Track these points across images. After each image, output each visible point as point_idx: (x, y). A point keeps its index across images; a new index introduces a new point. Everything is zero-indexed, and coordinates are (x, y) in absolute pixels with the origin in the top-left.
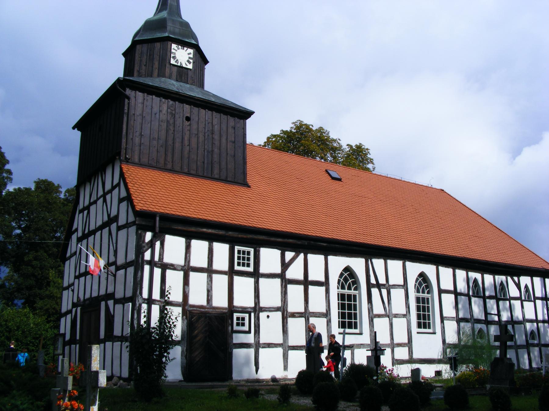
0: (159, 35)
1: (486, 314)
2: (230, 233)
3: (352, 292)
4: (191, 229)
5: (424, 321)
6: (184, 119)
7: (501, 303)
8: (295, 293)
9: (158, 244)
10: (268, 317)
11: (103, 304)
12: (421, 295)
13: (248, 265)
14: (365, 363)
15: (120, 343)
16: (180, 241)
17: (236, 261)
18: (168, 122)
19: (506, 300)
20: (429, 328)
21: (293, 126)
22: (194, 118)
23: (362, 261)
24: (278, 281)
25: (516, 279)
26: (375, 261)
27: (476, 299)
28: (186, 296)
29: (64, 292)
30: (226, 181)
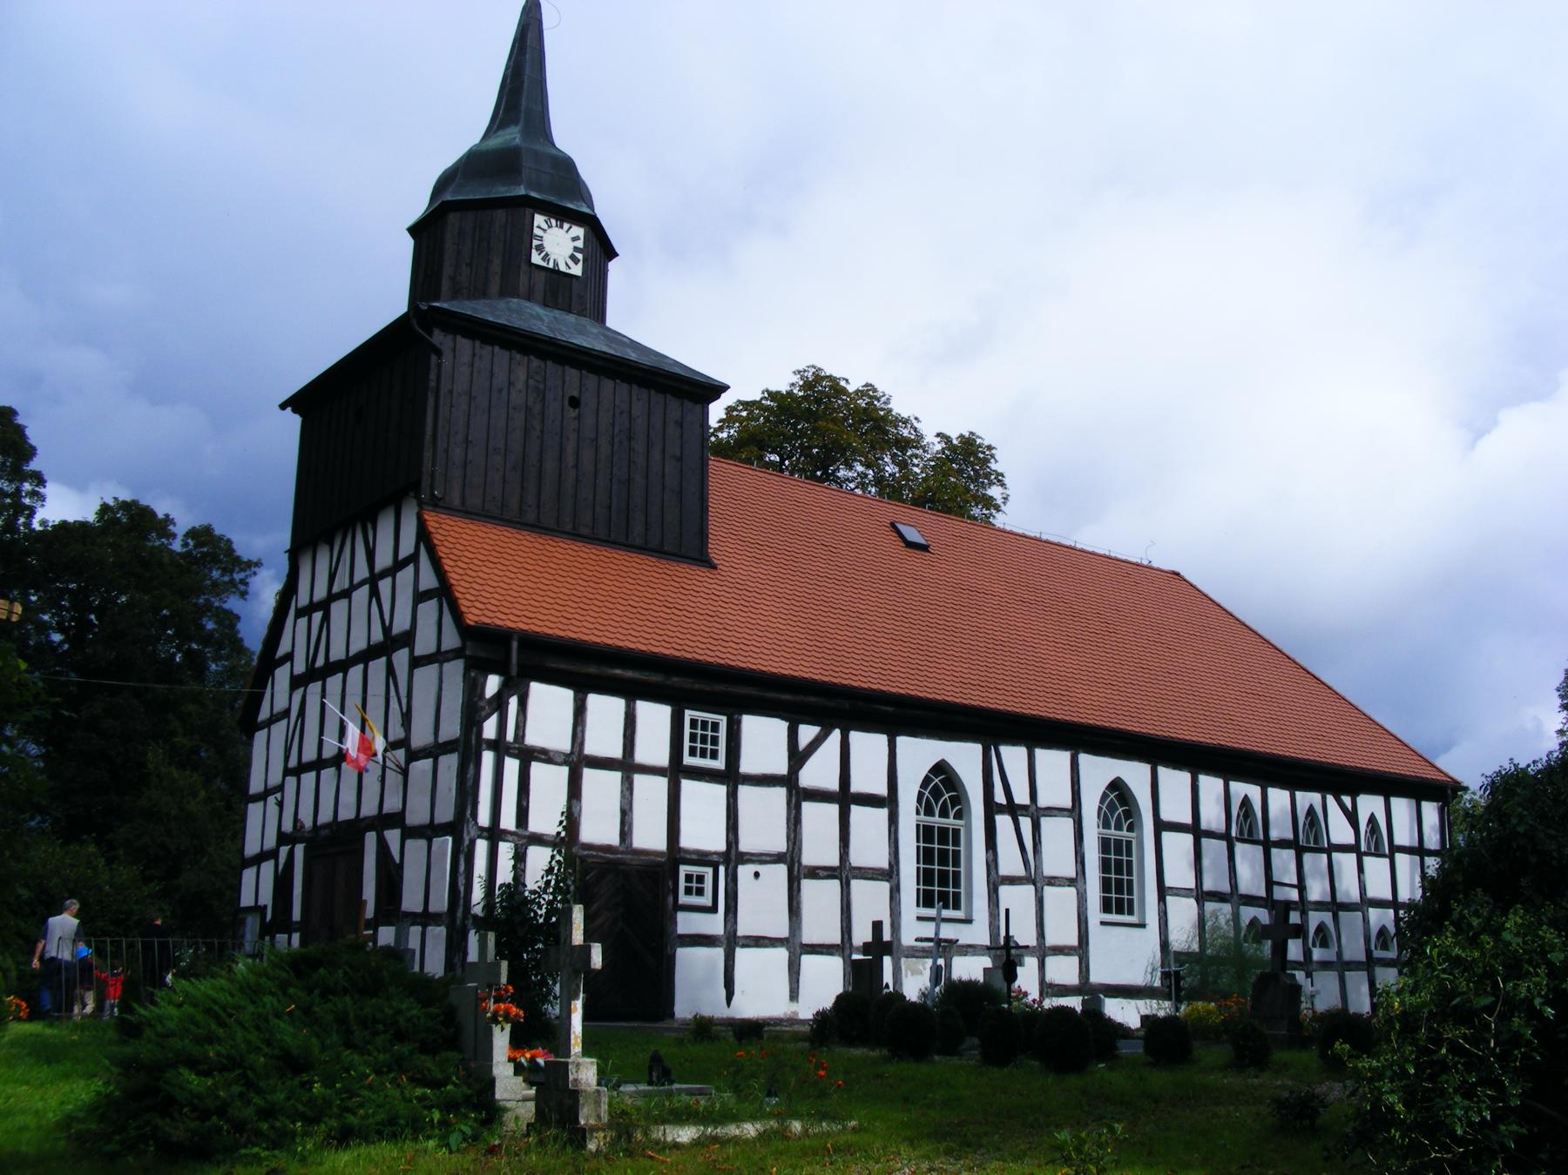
0: (503, 191)
1: (1270, 883)
2: (675, 679)
3: (950, 822)
8: (820, 819)
9: (513, 702)
10: (757, 875)
11: (371, 839)
12: (1112, 833)
13: (714, 755)
16: (563, 697)
17: (687, 744)
18: (528, 409)
19: (1320, 850)
20: (1131, 912)
21: (796, 379)
22: (589, 400)
23: (975, 749)
24: (780, 793)
25: (1347, 800)
27: (1247, 846)
28: (572, 820)
29: (251, 806)
30: (660, 552)
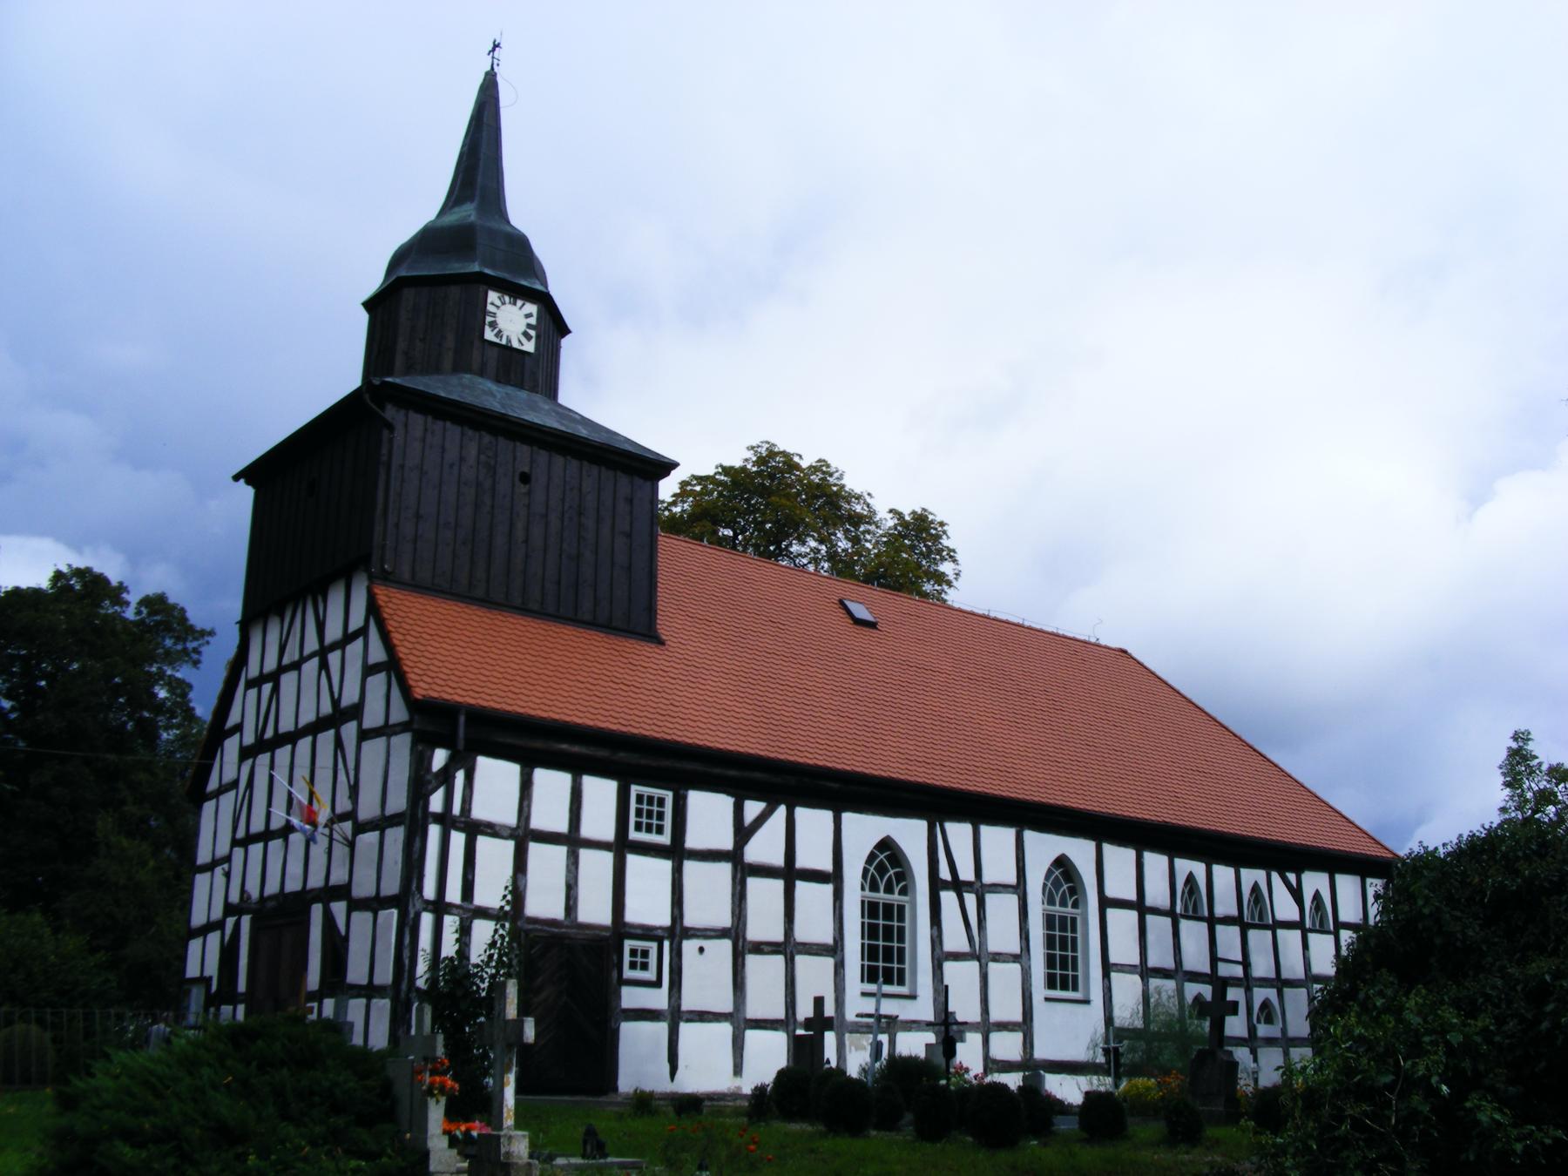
1: (1214, 959)
3: (895, 898)
4: (536, 744)
5: (1063, 974)
6: (517, 479)
7: (1253, 935)
8: (765, 895)
9: (460, 776)
10: (701, 950)
11: (317, 911)
13: (660, 830)
14: (922, 1054)
15: (364, 1001)
17: (632, 819)
18: (478, 484)
20: (1075, 989)
25: (1292, 877)
26: (951, 827)
